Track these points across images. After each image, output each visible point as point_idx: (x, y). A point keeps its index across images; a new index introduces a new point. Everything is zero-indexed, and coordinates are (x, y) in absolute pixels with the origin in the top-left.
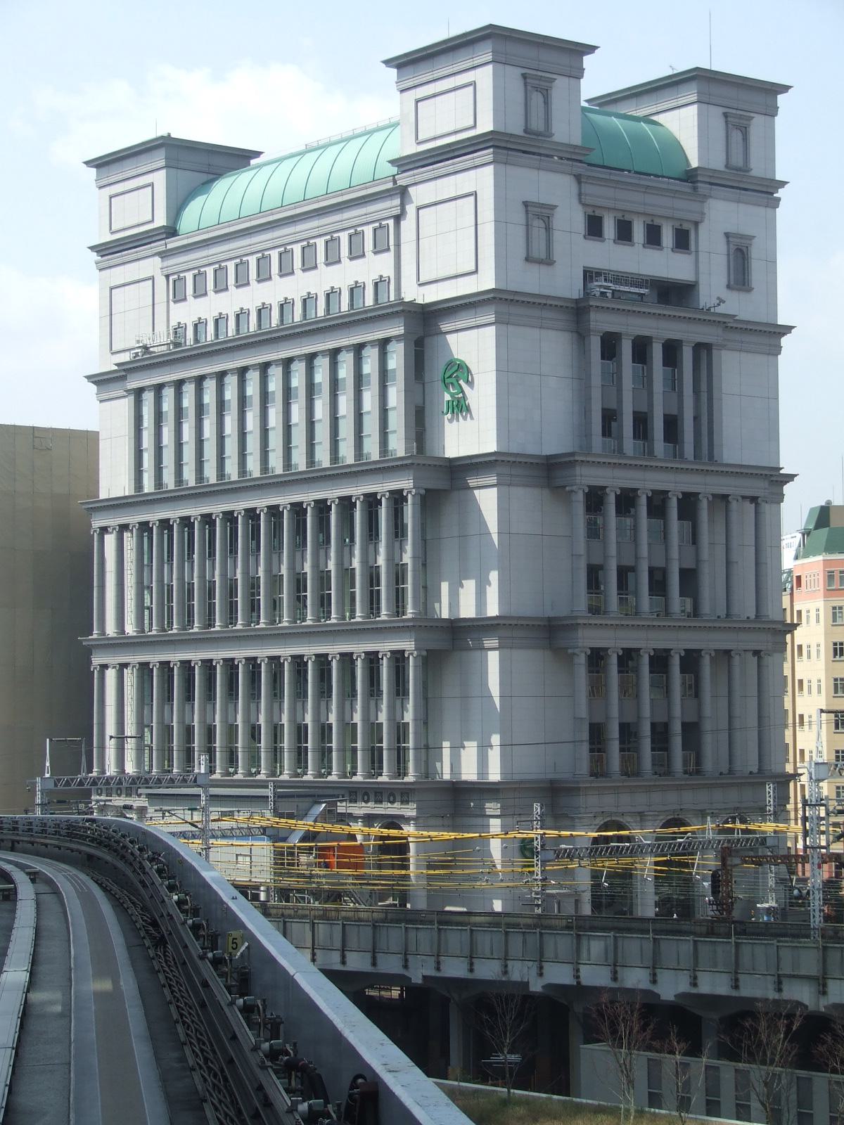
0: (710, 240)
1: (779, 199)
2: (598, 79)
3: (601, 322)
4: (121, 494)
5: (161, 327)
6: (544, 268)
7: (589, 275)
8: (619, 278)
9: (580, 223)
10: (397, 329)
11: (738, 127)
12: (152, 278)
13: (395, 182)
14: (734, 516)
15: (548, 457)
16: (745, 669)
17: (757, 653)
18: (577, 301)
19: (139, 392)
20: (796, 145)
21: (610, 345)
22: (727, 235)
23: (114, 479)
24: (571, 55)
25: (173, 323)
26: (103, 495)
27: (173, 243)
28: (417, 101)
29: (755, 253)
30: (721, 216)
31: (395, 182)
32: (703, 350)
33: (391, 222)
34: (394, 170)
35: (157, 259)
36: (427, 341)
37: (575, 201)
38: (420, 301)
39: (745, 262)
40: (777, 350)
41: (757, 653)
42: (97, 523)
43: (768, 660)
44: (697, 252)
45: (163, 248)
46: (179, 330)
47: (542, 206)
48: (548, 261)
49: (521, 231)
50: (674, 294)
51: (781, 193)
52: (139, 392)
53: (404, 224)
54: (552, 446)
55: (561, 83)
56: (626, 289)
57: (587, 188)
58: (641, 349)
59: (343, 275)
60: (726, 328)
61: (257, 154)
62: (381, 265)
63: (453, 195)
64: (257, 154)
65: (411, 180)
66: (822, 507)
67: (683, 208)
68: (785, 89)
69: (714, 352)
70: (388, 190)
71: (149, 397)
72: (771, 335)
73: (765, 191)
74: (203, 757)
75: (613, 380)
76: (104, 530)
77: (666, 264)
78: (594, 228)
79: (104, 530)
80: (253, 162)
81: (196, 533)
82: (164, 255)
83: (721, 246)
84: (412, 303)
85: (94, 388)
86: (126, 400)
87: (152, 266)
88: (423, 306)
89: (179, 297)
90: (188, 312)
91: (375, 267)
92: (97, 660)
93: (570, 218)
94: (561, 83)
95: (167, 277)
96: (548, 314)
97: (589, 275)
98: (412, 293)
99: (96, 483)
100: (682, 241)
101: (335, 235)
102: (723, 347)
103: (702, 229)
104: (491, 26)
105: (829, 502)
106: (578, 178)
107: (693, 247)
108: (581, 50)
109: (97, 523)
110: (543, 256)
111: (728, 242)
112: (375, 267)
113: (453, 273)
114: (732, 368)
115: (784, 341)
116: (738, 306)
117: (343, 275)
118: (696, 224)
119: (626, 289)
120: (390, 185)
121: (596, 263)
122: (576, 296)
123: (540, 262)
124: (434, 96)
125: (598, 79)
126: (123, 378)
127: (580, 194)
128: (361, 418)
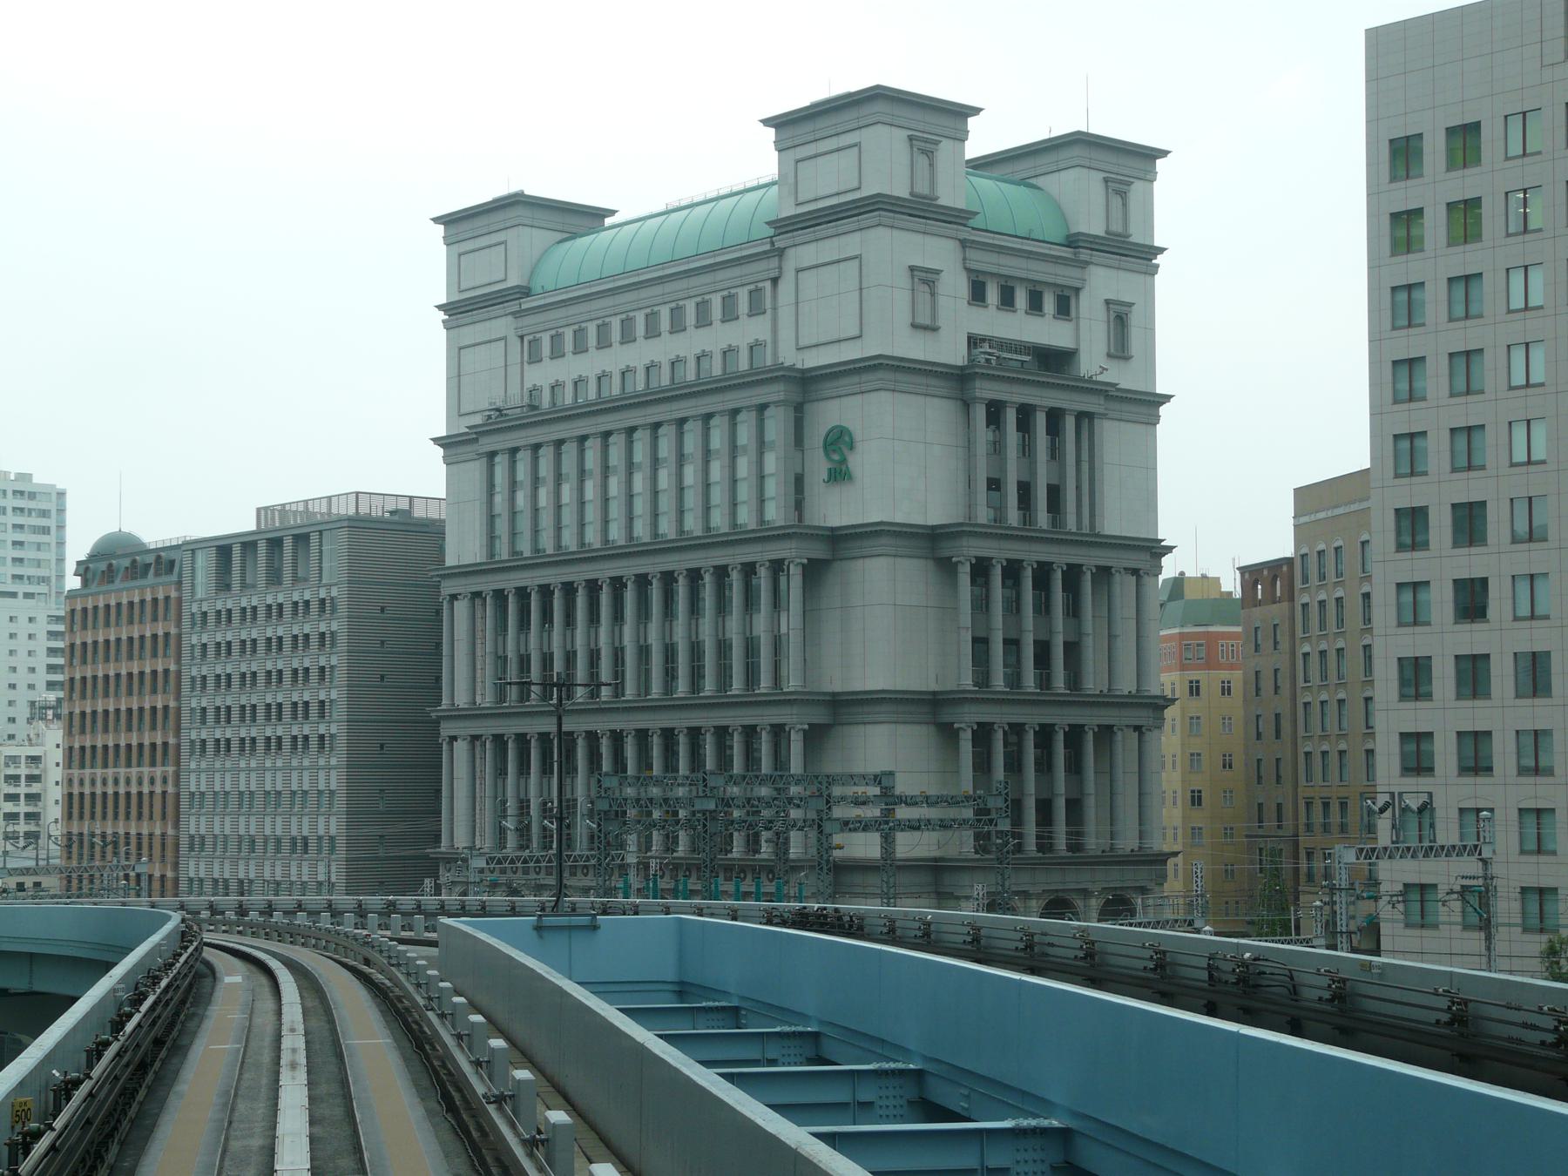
0: (1090, 306)
1: (1157, 266)
2: (981, 140)
3: (986, 390)
4: (472, 561)
5: (514, 389)
6: (929, 335)
7: (973, 341)
8: (1004, 345)
9: (962, 287)
10: (774, 392)
11: (1118, 192)
12: (505, 338)
13: (772, 243)
14: (1117, 589)
15: (933, 527)
16: (1125, 744)
17: (1138, 728)
18: (962, 368)
19: (492, 455)
20: (1173, 211)
21: (995, 413)
22: (1108, 302)
23: (463, 548)
24: (958, 114)
25: (528, 385)
26: (450, 561)
27: (527, 304)
28: (797, 161)
29: (1135, 319)
30: (1102, 283)
31: (772, 243)
32: (1085, 418)
33: (768, 285)
34: (771, 232)
35: (510, 318)
36: (807, 407)
37: (959, 266)
38: (799, 366)
39: (1126, 327)
40: (1154, 420)
41: (1138, 728)
42: (448, 588)
43: (1149, 736)
44: (1078, 318)
45: (516, 308)
46: (535, 391)
47: (928, 271)
48: (933, 329)
49: (907, 295)
50: (1055, 361)
51: (1159, 260)
52: (492, 455)
53: (782, 285)
54: (935, 515)
55: (946, 145)
56: (1009, 356)
57: (971, 254)
58: (1025, 415)
59: (716, 338)
60: (1108, 397)
61: (612, 213)
62: (758, 329)
63: (836, 258)
64: (612, 213)
65: (790, 242)
66: (1175, 579)
67: (1065, 275)
68: (1164, 153)
69: (1096, 421)
70: (765, 252)
71: (501, 463)
72: (1149, 404)
73: (1143, 256)
74: (461, 841)
75: (997, 448)
76: (454, 597)
77: (1047, 331)
78: (977, 294)
79: (454, 597)
80: (608, 221)
81: (526, 598)
82: (516, 315)
83: (1101, 313)
84: (791, 368)
85: (440, 451)
86: (477, 463)
87: (502, 326)
88: (803, 371)
89: (535, 359)
90: (543, 375)
91: (746, 331)
92: (447, 729)
93: (955, 284)
94: (946, 145)
95: (522, 337)
96: (932, 381)
97: (973, 341)
98: (789, 356)
99: (441, 550)
100: (1064, 309)
101: (707, 297)
102: (1104, 416)
103: (1083, 296)
104: (878, 87)
105: (1182, 573)
106: (964, 244)
107: (1073, 313)
108: (961, 113)
109: (448, 588)
110: (927, 322)
111: (1108, 310)
112: (746, 331)
113: (836, 337)
114: (1113, 436)
115: (1163, 410)
116: (1123, 377)
117: (716, 338)
118: (1077, 290)
119: (1009, 356)
120: (768, 247)
121: (981, 330)
122: (960, 363)
123: (925, 328)
124: (816, 156)
125: (981, 140)
126: (476, 440)
127: (964, 259)
128: (734, 486)
